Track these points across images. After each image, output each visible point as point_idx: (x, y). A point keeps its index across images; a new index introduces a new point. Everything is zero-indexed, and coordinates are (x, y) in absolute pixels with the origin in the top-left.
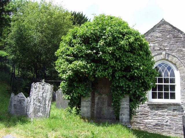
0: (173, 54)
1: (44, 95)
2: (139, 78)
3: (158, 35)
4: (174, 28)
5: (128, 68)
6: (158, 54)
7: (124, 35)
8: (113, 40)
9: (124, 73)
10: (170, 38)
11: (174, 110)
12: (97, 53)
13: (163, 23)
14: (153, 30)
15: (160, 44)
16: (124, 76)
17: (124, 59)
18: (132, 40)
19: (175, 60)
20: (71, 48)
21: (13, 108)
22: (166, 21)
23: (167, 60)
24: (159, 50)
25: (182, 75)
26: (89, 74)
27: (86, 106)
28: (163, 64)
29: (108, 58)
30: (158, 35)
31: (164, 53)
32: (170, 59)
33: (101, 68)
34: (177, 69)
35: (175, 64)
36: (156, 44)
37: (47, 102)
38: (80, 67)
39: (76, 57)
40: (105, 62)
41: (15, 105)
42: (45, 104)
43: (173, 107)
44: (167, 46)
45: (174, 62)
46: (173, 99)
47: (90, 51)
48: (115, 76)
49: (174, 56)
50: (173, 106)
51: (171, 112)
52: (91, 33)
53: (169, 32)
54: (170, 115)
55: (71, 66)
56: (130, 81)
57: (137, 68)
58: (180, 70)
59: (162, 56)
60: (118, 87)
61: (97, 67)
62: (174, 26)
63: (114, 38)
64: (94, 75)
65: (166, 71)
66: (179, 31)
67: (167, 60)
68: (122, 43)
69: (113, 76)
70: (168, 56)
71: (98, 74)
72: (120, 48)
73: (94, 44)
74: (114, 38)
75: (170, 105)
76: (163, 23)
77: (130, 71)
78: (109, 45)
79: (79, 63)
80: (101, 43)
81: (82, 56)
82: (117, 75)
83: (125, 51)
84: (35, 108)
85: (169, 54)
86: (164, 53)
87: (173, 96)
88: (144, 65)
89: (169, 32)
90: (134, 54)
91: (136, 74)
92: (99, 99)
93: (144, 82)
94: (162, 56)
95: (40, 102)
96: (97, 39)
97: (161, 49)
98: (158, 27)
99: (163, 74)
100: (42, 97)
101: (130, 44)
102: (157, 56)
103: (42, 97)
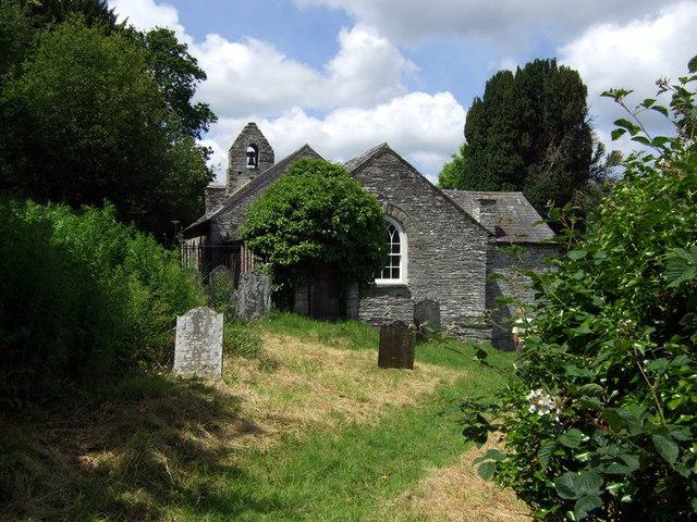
3: (378, 171)
4: (404, 162)
10: (395, 179)
11: (398, 296)
15: (380, 186)
19: (401, 215)
23: (390, 215)
27: (301, 300)
29: (343, 239)
43: (396, 292)
46: (398, 365)
51: (394, 300)
53: (395, 167)
54: (391, 304)
66: (410, 166)
67: (390, 215)
71: (329, 258)
72: (358, 226)
75: (392, 288)
86: (385, 203)
87: (396, 274)
89: (395, 167)
91: (675, 311)
92: (316, 287)
95: (254, 298)
96: (330, 213)
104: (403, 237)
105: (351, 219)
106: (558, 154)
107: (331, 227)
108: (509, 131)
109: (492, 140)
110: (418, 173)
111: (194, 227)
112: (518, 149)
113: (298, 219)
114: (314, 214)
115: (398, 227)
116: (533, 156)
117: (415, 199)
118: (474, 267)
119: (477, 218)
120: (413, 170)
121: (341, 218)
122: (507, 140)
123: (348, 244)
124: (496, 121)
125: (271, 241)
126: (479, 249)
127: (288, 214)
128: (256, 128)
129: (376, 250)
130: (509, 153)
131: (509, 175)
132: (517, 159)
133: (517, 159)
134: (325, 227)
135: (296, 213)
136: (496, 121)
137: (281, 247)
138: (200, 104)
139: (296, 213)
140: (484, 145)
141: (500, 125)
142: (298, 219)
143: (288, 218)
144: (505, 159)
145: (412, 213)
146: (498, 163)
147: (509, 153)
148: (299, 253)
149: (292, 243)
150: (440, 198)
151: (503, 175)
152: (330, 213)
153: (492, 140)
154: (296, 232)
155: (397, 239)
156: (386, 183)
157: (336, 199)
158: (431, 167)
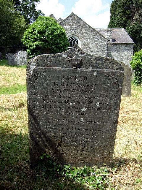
0: (78, 32)
1: (24, 56)
2: (62, 47)
3: (70, 21)
4: (78, 17)
5: (58, 44)
6: (70, 32)
7: (55, 30)
8: (51, 32)
9: (56, 45)
10: (76, 23)
12: (45, 38)
13: (73, 14)
14: (67, 18)
16: (56, 47)
17: (56, 40)
18: (59, 32)
19: (78, 35)
20: (33, 36)
21: (10, 62)
22: (74, 13)
23: (75, 35)
24: (71, 30)
25: (82, 42)
26: (42, 46)
28: (73, 37)
29: (50, 40)
30: (70, 21)
31: (73, 31)
32: (76, 34)
33: (47, 44)
34: (80, 39)
35: (79, 37)
36: (69, 26)
37: (26, 59)
38: (39, 44)
39: (36, 40)
40: (48, 42)
41: (10, 61)
42: (25, 60)
44: (75, 27)
45: (78, 36)
47: (43, 38)
48: (52, 47)
49: (78, 33)
50: (125, 46)
52: (43, 30)
53: (76, 20)
55: (34, 43)
56: (58, 48)
57: (61, 44)
58: (81, 40)
59: (72, 33)
60: (53, 51)
61: (45, 43)
62: (79, 16)
63: (52, 32)
64: (44, 47)
65: (74, 41)
66: (81, 19)
67: (75, 35)
68: (55, 34)
69: (52, 47)
70: (75, 33)
71: (46, 47)
72: (54, 36)
73: (43, 34)
74: (52, 32)
76: (73, 14)
77: (58, 45)
78: (49, 34)
79: (38, 42)
80: (47, 34)
81: (39, 39)
82: (53, 46)
83: (56, 36)
84: (20, 62)
85: (75, 32)
86: (73, 31)
88: (63, 42)
89: (76, 20)
90: (60, 37)
93: (64, 48)
94: (72, 33)
95: (22, 59)
96: (45, 32)
97: (71, 29)
98: (70, 17)
99: (73, 42)
100: (23, 57)
101: (58, 34)
102: (70, 33)
103: (23, 57)
104: (79, 41)
105: (52, 33)
106: (138, 16)
107: (45, 36)
108: (122, 9)
109: (117, 13)
110: (84, 21)
111: (60, 70)
112: (125, 15)
113: (35, 34)
114: (40, 32)
115: (78, 39)
116: (130, 17)
117: (83, 29)
118: (103, 50)
119: (106, 37)
120: (82, 20)
121: (48, 33)
122: (121, 12)
123: (52, 42)
124: (118, 7)
125: (28, 42)
126: (105, 45)
127: (32, 33)
128: (53, 16)
129: (61, 44)
130: (122, 16)
131: (122, 24)
132: (124, 18)
133: (124, 18)
134: (43, 36)
135: (34, 32)
136: (118, 7)
137: (31, 43)
138: (39, 10)
139: (34, 32)
140: (115, 15)
141: (119, 8)
142: (35, 34)
143: (32, 34)
144: (120, 19)
145: (82, 34)
146: (119, 20)
147: (122, 16)
148: (35, 45)
149: (34, 42)
150: (91, 29)
151: (119, 24)
152: (45, 32)
153: (117, 13)
154: (35, 39)
155: (78, 42)
156: (73, 25)
157: (47, 27)
158: (36, 4)
